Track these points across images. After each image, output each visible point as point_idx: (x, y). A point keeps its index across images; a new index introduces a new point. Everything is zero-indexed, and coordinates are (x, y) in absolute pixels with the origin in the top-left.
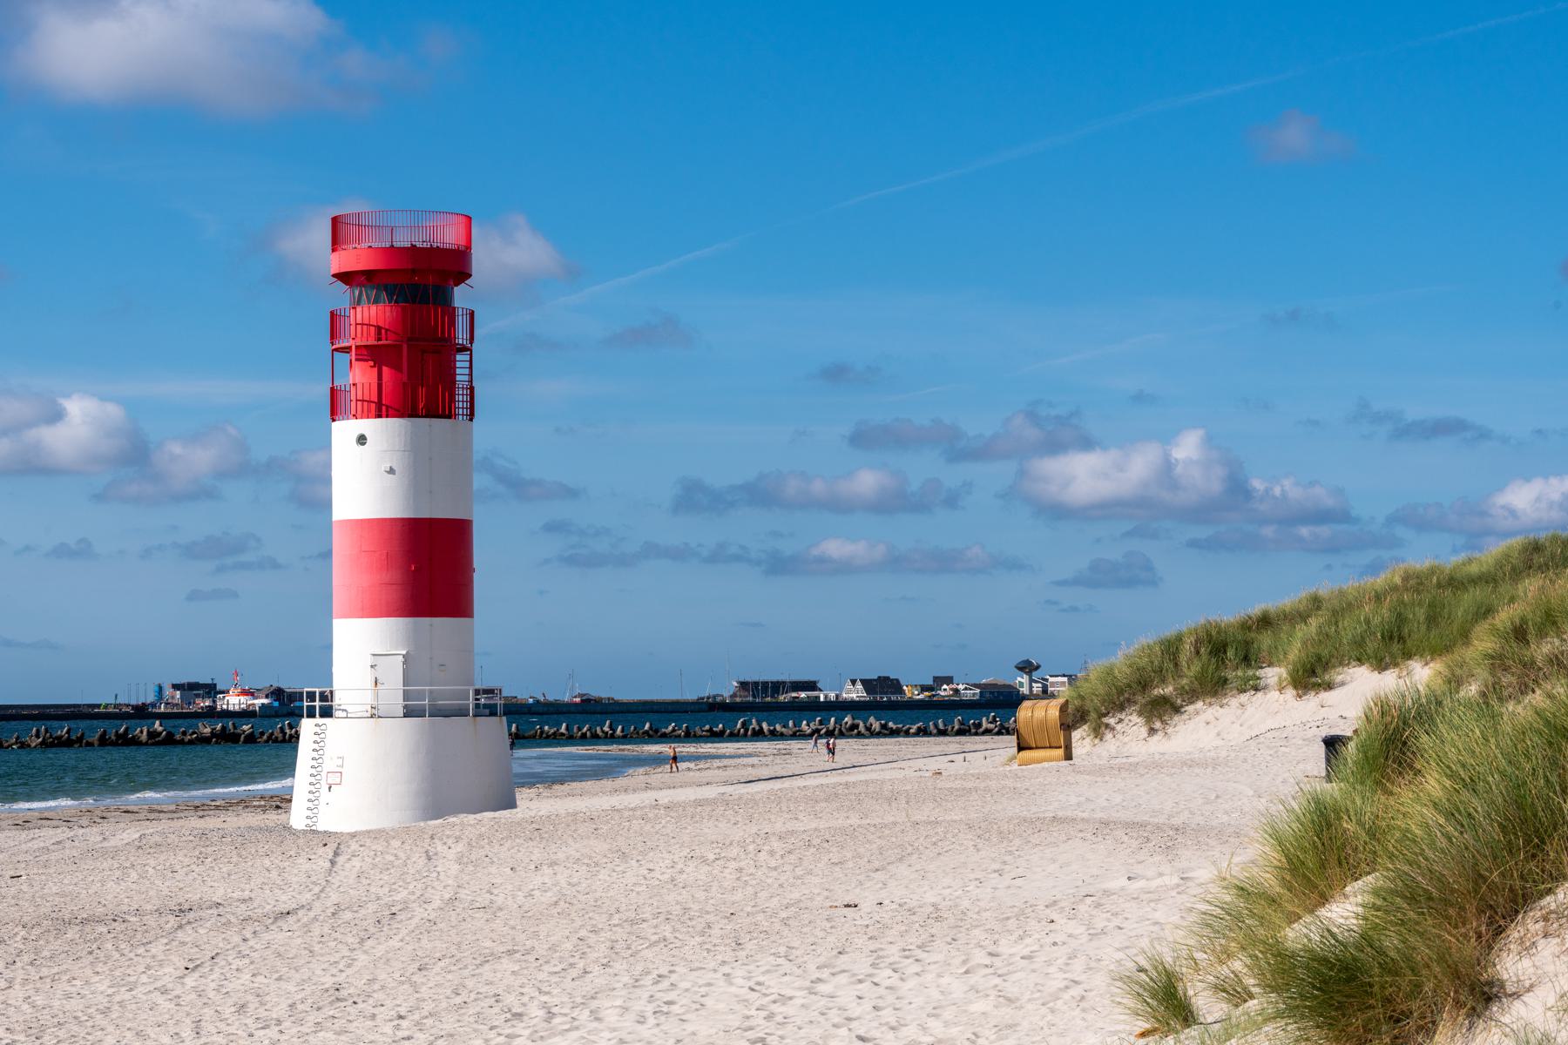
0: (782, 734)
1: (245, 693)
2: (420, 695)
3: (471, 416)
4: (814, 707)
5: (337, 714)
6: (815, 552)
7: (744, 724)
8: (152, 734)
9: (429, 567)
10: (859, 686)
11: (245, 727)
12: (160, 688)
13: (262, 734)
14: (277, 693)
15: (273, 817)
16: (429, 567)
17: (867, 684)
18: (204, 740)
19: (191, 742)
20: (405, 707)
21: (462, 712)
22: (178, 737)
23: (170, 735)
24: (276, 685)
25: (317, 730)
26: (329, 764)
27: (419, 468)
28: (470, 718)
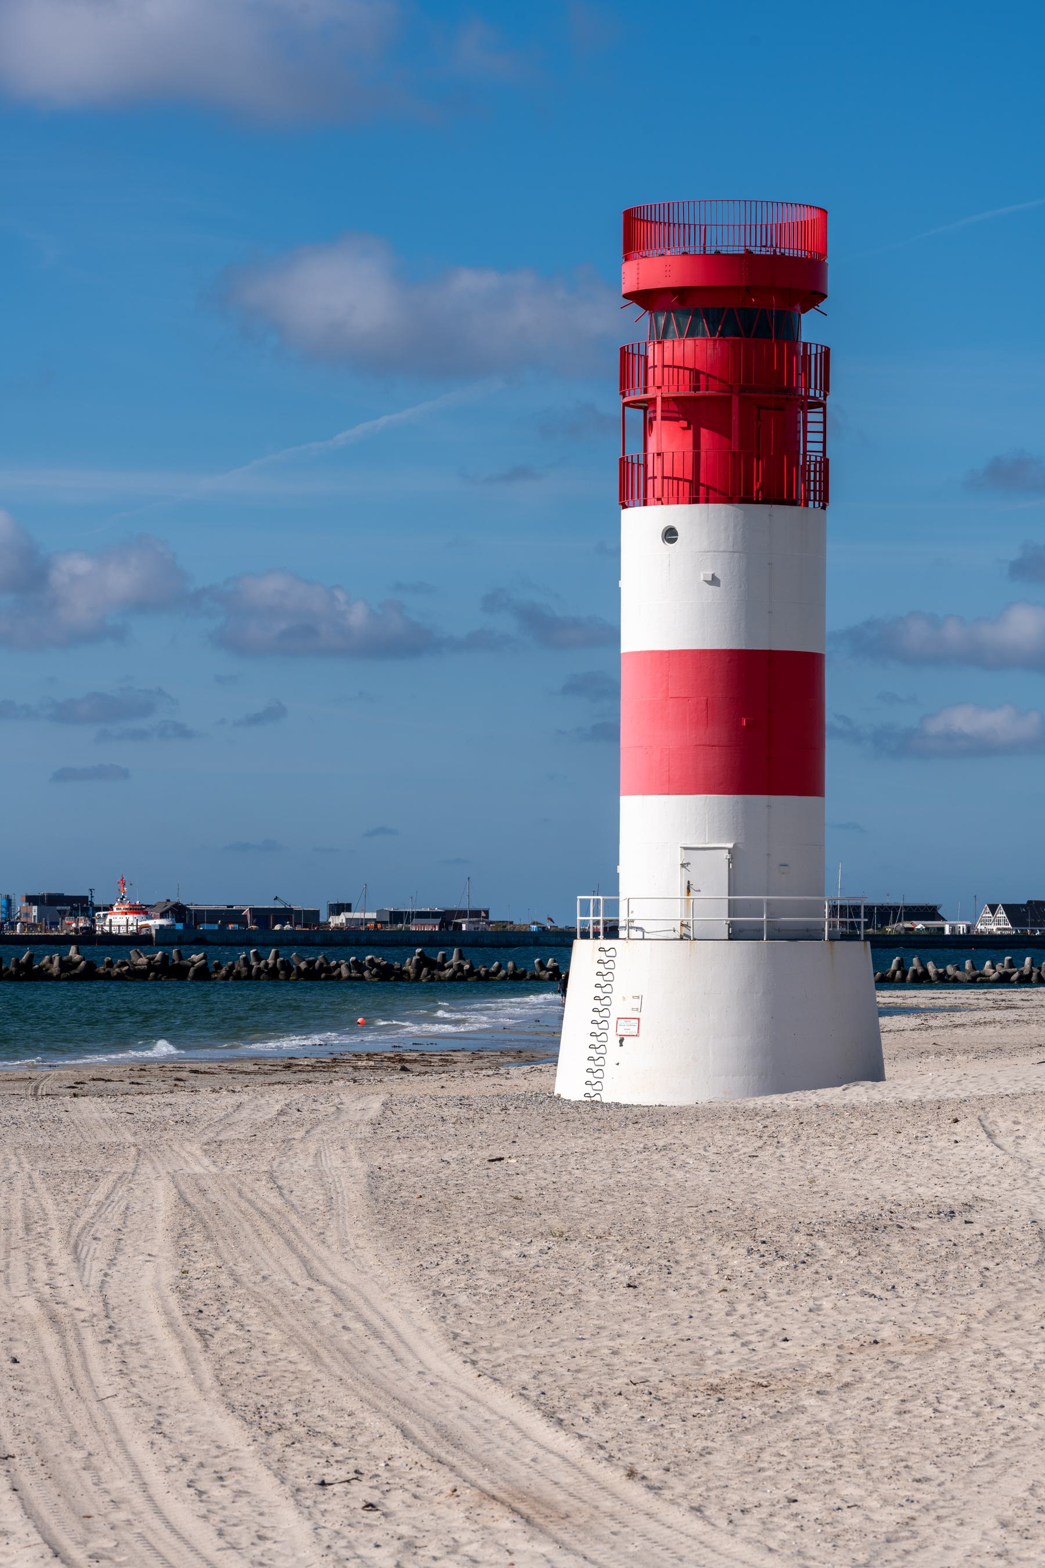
0: (956, 980)
1: (135, 910)
2: (754, 908)
3: (824, 501)
4: (935, 942)
5: (623, 934)
6: (935, 727)
7: (900, 964)
8: (66, 965)
9: (762, 721)
10: (1001, 914)
11: (194, 957)
12: (9, 901)
13: (218, 967)
14: (178, 911)
15: (519, 1080)
16: (762, 721)
17: (1013, 912)
18: (137, 975)
19: (120, 977)
20: (731, 925)
21: (811, 934)
22: (101, 969)
23: (91, 966)
24: (174, 900)
25: (602, 956)
26: (619, 1007)
27: (755, 579)
28: (825, 943)
